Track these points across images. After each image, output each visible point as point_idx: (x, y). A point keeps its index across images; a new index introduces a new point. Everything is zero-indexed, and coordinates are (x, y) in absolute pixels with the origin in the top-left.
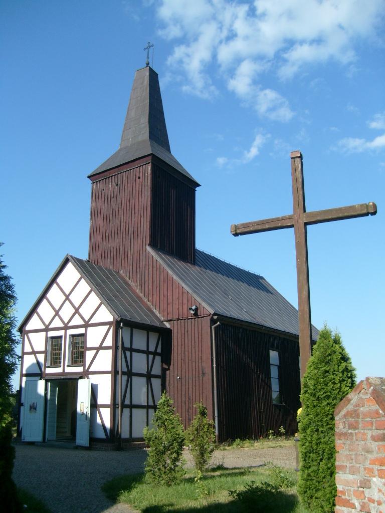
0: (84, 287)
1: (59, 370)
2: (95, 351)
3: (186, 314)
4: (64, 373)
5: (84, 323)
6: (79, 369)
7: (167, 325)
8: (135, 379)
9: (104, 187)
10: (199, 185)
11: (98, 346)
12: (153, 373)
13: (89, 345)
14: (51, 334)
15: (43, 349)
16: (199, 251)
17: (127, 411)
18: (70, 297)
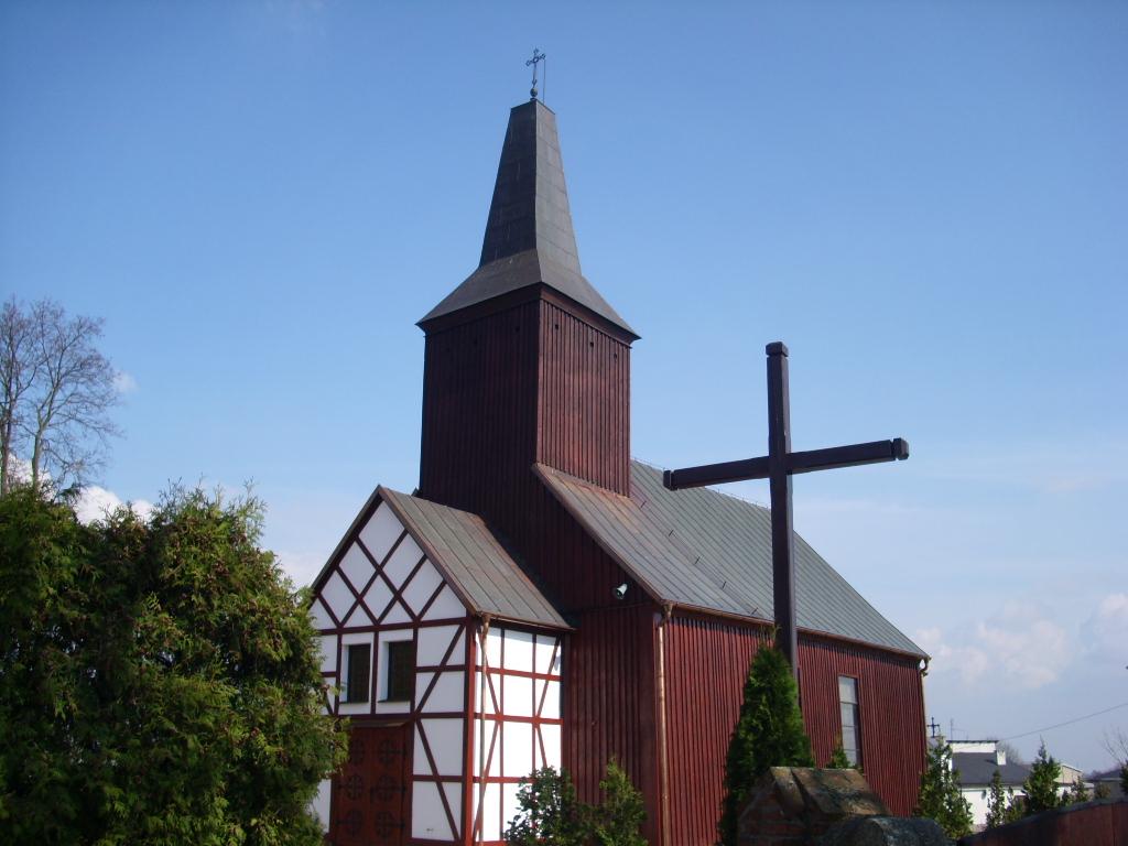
1: (365, 709)
2: (449, 663)
6: (403, 708)
10: (638, 338)
12: (543, 716)
13: (421, 662)
14: (349, 640)
15: (334, 669)
16: (640, 465)
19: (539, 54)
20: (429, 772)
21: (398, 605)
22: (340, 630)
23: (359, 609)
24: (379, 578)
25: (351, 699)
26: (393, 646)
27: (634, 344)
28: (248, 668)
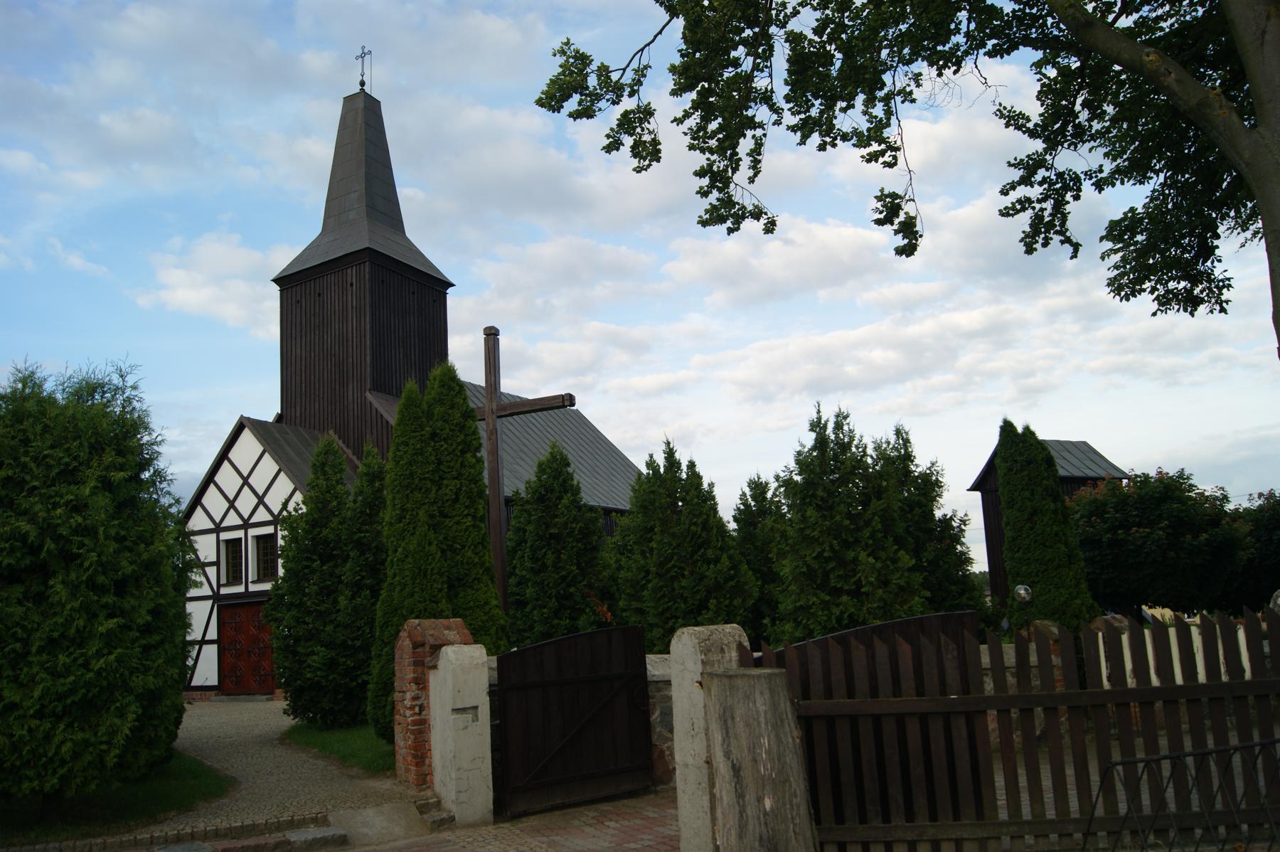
0: (269, 465)
1: (240, 589)
4: (247, 593)
5: (241, 523)
9: (298, 298)
10: (453, 285)
14: (225, 536)
15: (214, 559)
21: (261, 508)
22: (218, 529)
23: (232, 512)
24: (246, 488)
25: (229, 583)
26: (258, 538)
27: (450, 291)
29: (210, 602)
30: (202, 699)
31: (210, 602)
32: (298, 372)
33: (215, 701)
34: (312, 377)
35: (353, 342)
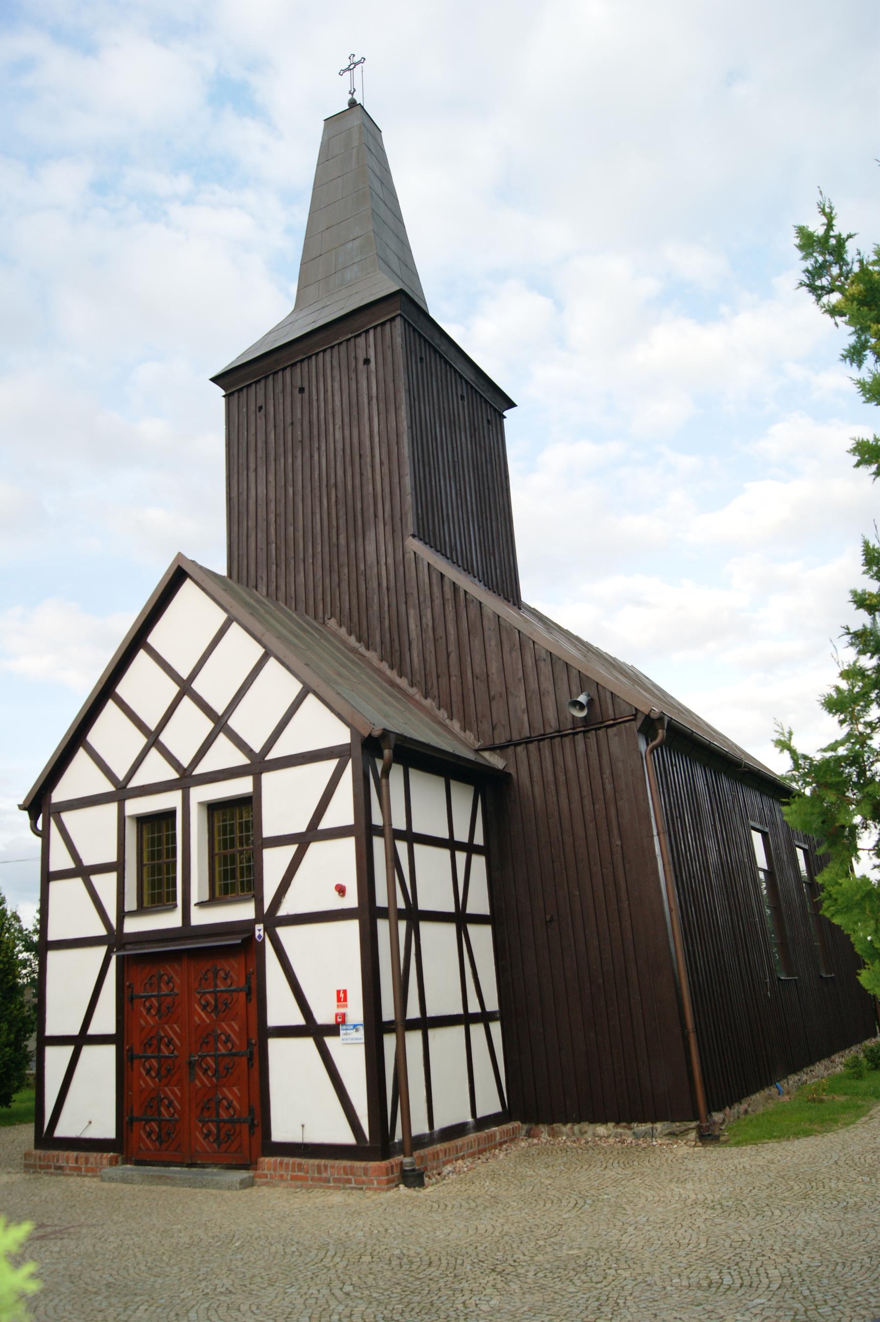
1: (171, 920)
2: (292, 849)
3: (611, 712)
4: (187, 930)
7: (496, 761)
8: (425, 928)
9: (261, 402)
10: (511, 405)
11: (303, 829)
12: (470, 910)
14: (136, 807)
15: (112, 857)
17: (414, 1039)
18: (143, 741)
19: (356, 59)
20: (95, 879)
26: (213, 808)
28: (845, 1124)
29: (102, 951)
30: (78, 1169)
31: (102, 951)
32: (262, 524)
33: (112, 1180)
34: (291, 529)
35: (373, 457)
